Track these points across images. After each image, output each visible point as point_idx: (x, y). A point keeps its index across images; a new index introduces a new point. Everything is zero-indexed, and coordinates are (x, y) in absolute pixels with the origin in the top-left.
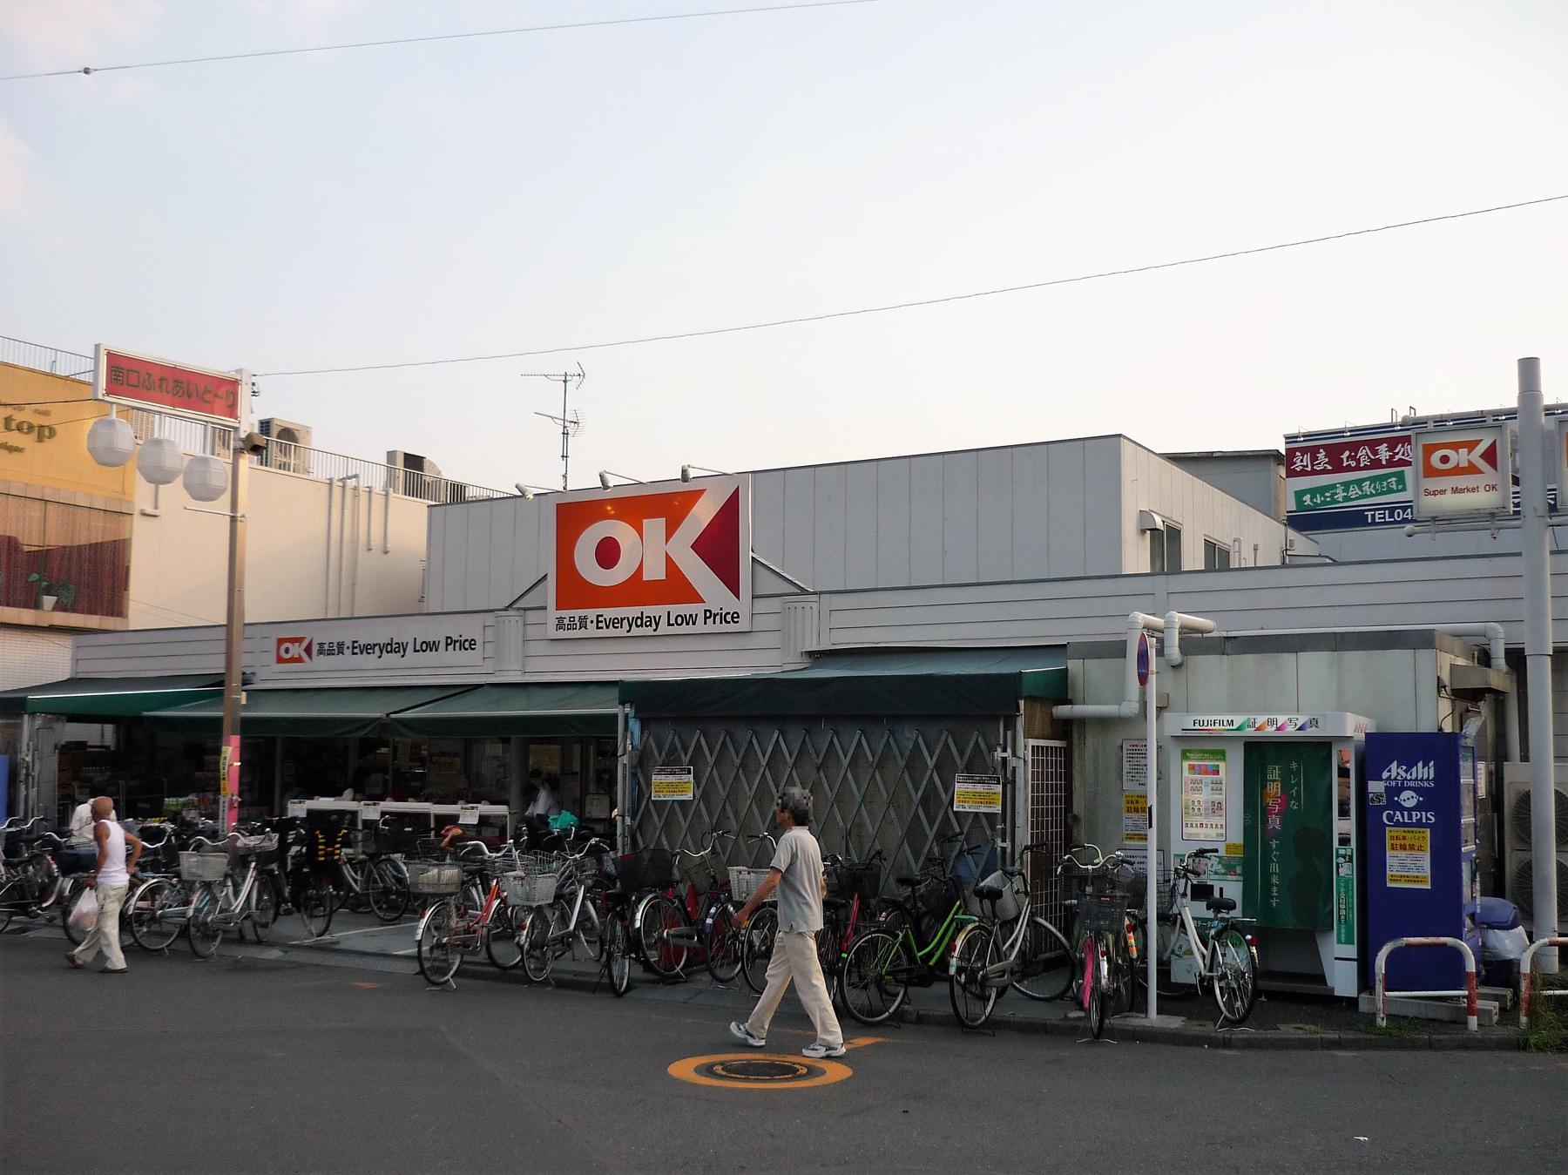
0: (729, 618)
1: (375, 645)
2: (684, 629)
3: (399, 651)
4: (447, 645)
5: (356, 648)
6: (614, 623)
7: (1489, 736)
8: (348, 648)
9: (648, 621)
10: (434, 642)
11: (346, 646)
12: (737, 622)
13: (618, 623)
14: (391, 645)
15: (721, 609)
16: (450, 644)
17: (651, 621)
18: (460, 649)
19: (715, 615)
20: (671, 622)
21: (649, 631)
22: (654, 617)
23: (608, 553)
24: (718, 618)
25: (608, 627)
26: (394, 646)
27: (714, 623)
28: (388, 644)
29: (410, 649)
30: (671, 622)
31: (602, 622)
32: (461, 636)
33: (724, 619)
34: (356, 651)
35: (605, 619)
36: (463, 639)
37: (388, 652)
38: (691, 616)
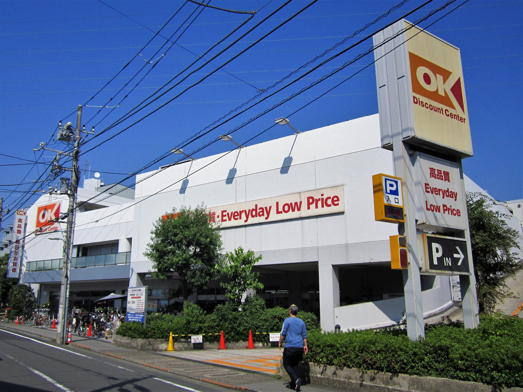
0: (329, 202)
1: (440, 190)
2: (291, 215)
3: (263, 215)
4: (309, 204)
5: (225, 216)
6: (435, 191)
7: (243, 374)
8: (218, 217)
9: (236, 216)
10: (437, 206)
11: (216, 216)
12: (338, 204)
13: (238, 215)
14: (256, 210)
15: (322, 195)
16: (312, 203)
17: (263, 212)
18: (323, 206)
19: (317, 201)
20: (279, 211)
21: (262, 219)
22: (266, 208)
23: (19, 213)
24: (320, 203)
25: (230, 219)
26: (258, 211)
27: (317, 207)
28: (446, 191)
29: (273, 211)
30: (279, 211)
31: (428, 188)
32: (451, 206)
33: (325, 203)
34: (224, 218)
35: (228, 214)
36: (325, 197)
37: (253, 216)
38: (437, 206)
